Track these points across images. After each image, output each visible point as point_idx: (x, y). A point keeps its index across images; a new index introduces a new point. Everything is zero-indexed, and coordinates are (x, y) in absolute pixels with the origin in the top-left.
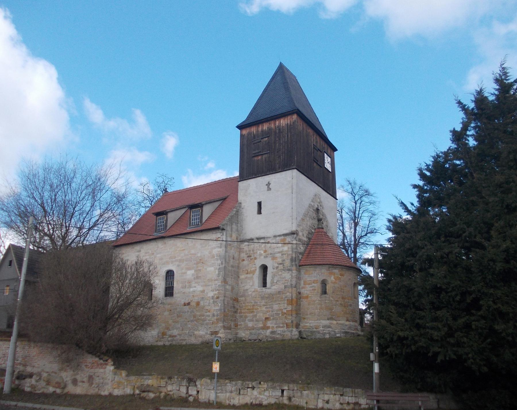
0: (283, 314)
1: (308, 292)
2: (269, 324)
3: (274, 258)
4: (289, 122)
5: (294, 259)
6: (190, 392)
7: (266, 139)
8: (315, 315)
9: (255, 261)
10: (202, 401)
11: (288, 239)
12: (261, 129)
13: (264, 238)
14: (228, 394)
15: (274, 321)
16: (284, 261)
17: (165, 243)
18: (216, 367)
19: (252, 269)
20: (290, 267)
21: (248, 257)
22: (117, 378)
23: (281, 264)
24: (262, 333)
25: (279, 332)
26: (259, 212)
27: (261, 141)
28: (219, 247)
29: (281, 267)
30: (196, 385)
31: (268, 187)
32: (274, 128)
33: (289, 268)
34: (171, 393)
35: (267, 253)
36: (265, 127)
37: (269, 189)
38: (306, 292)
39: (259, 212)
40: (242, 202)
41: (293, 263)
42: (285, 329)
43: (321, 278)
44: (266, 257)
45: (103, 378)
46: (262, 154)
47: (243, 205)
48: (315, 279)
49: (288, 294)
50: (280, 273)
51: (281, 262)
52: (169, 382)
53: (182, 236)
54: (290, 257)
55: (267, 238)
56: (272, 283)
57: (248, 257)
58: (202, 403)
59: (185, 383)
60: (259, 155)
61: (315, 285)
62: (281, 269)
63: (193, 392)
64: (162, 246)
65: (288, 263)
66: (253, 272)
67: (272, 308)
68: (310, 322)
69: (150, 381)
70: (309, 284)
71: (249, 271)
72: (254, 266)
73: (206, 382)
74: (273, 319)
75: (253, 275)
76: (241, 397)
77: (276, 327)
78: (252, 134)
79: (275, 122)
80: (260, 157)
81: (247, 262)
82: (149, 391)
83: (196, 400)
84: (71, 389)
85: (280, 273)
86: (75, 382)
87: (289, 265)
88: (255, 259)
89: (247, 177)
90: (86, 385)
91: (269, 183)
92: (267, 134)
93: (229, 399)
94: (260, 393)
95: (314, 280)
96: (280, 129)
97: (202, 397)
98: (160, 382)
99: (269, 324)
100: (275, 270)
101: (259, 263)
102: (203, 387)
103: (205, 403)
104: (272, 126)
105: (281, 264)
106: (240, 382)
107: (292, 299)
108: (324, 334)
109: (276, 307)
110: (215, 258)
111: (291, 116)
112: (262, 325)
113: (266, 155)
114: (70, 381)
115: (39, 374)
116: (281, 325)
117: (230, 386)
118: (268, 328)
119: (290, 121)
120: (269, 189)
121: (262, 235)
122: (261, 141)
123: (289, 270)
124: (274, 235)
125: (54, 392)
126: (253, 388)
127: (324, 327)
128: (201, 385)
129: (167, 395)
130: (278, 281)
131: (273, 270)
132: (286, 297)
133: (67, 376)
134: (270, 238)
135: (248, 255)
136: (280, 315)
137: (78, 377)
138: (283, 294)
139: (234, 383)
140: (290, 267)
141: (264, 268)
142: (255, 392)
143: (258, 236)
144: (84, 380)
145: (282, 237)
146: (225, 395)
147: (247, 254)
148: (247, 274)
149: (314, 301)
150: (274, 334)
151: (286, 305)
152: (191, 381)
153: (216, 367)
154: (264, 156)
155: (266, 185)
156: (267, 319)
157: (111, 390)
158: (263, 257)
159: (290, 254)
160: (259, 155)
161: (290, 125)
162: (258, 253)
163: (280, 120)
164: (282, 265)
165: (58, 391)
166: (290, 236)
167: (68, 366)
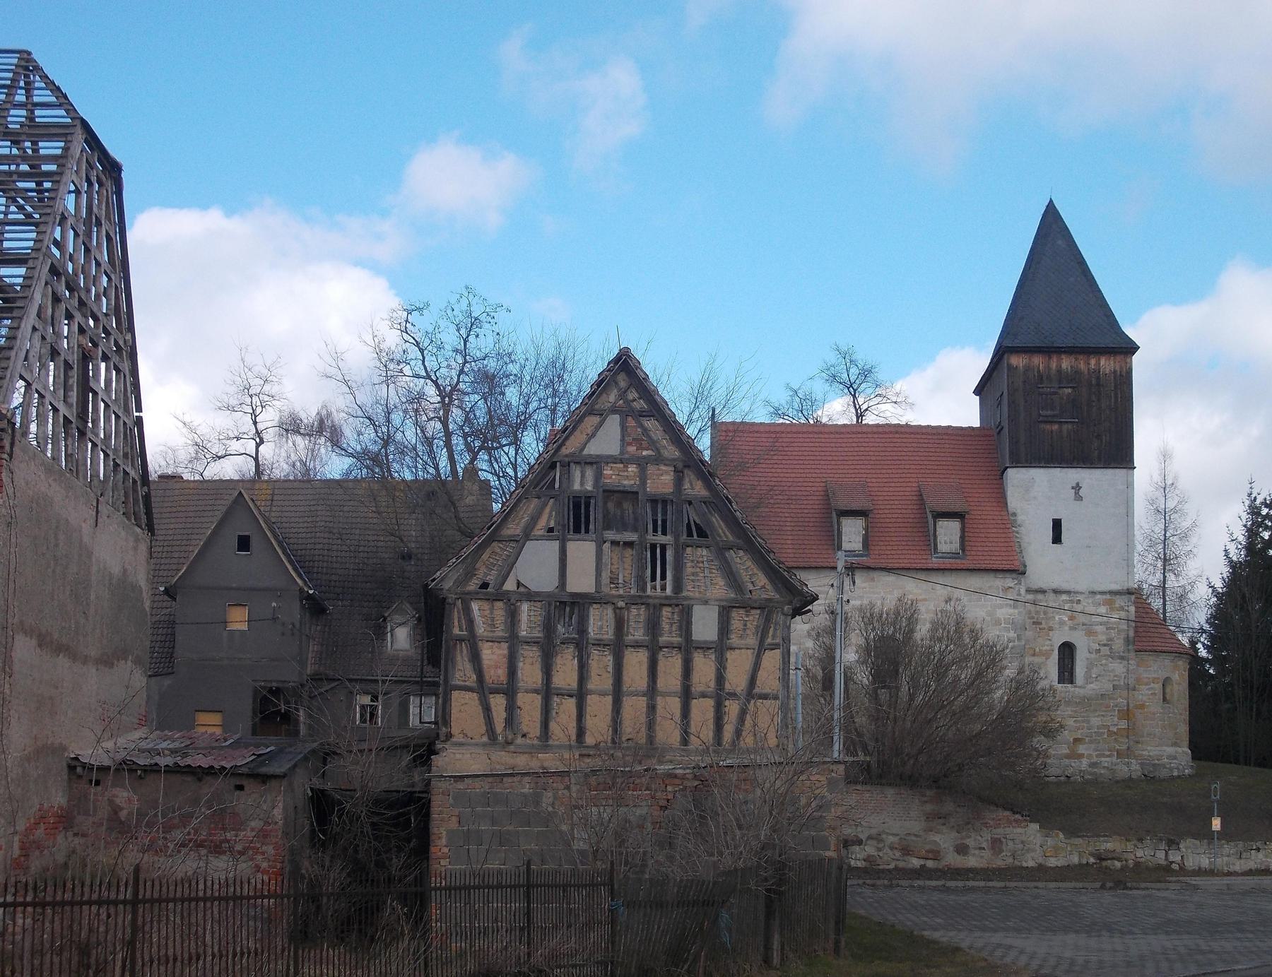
0: (1111, 733)
1: (1145, 698)
2: (1081, 749)
3: (1090, 633)
4: (1118, 368)
5: (1131, 639)
6: (1171, 858)
7: (1070, 390)
8: (1155, 735)
9: (1051, 633)
10: (1190, 869)
11: (1120, 601)
12: (1057, 366)
13: (1068, 592)
14: (1225, 859)
15: (1093, 746)
16: (1111, 640)
17: (873, 580)
18: (1216, 824)
19: (1045, 648)
20: (1123, 652)
21: (1034, 623)
22: (1050, 842)
23: (1105, 645)
24: (1073, 764)
25: (1106, 765)
26: (1057, 539)
27: (1055, 393)
28: (1011, 605)
29: (1105, 650)
30: (1179, 849)
31: (1075, 493)
32: (1086, 372)
33: (1121, 654)
34: (1143, 860)
35: (1076, 622)
36: (1066, 363)
37: (1078, 497)
38: (1140, 697)
39: (1057, 539)
40: (1018, 511)
41: (1131, 647)
42: (1114, 759)
43: (1163, 674)
44: (1073, 628)
45: (1023, 842)
46: (1061, 422)
47: (1020, 518)
48: (1155, 676)
49: (1120, 700)
50: (1104, 662)
51: (1105, 642)
52: (1140, 845)
53: (922, 576)
54: (1123, 636)
55: (1077, 593)
56: (1088, 678)
57: (1034, 623)
58: (1189, 871)
59: (1163, 846)
60: (1055, 422)
61: (1156, 686)
62: (1105, 656)
63: (1175, 857)
64: (864, 585)
65: (1119, 645)
66: (1047, 655)
67: (1088, 722)
68: (1149, 748)
69: (1109, 845)
70: (1146, 684)
71: (1037, 650)
72: (1048, 642)
73: (1193, 844)
74: (1091, 742)
75: (1046, 659)
76: (1242, 861)
77: (1097, 756)
78: (1036, 370)
79: (1089, 359)
80: (1056, 427)
81: (1031, 633)
82: (1113, 859)
83: (1182, 868)
84: (952, 859)
85: (1104, 662)
86: (962, 850)
87: (1122, 649)
88: (1051, 629)
89: (1027, 461)
90: (987, 854)
91: (1078, 484)
92: (1073, 378)
93: (1227, 865)
94: (1266, 857)
95: (1155, 678)
96: (1098, 378)
97: (1190, 864)
98: (1126, 846)
99: (1081, 749)
100: (1093, 656)
101: (1058, 639)
102: (1190, 851)
103: (1194, 870)
104: (1082, 366)
105: (1105, 645)
106: (1241, 844)
107: (1128, 710)
108: (1171, 769)
109: (1095, 721)
110: (1003, 625)
111: (1122, 356)
112: (1067, 751)
113: (1070, 426)
114: (951, 849)
115: (877, 838)
116: (1108, 753)
117: (1227, 848)
118: (1081, 756)
119: (1121, 368)
120: (1078, 497)
121: (1065, 586)
122: (1055, 393)
123: (1122, 658)
124: (1091, 590)
125: (923, 866)
126: (1258, 850)
127: (1169, 757)
128: (1187, 848)
129: (1137, 864)
130: (1099, 675)
131: (1088, 655)
132: (1116, 706)
133: (944, 840)
134: (1082, 593)
135: (1035, 620)
136: (1106, 736)
137: (970, 842)
138: (1110, 699)
139: (1232, 844)
140: (1123, 652)
141: (1067, 651)
142: (1260, 855)
143: (1055, 585)
144: (983, 846)
145: (1108, 597)
146: (1220, 860)
147: (1033, 618)
148: (1034, 655)
149: (1154, 714)
150: (1097, 768)
151: (1116, 719)
152: (1172, 843)
153: (1216, 824)
154: (1065, 427)
155: (1073, 488)
156: (1076, 740)
157: (1041, 860)
158: (1067, 628)
159: (1124, 630)
160: (1055, 422)
161: (1121, 375)
162: (1057, 619)
163: (1099, 360)
164: (1107, 648)
165: (930, 864)
166: (1123, 597)
167: (944, 824)
